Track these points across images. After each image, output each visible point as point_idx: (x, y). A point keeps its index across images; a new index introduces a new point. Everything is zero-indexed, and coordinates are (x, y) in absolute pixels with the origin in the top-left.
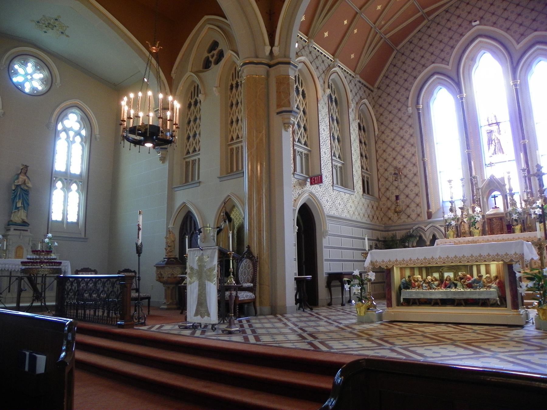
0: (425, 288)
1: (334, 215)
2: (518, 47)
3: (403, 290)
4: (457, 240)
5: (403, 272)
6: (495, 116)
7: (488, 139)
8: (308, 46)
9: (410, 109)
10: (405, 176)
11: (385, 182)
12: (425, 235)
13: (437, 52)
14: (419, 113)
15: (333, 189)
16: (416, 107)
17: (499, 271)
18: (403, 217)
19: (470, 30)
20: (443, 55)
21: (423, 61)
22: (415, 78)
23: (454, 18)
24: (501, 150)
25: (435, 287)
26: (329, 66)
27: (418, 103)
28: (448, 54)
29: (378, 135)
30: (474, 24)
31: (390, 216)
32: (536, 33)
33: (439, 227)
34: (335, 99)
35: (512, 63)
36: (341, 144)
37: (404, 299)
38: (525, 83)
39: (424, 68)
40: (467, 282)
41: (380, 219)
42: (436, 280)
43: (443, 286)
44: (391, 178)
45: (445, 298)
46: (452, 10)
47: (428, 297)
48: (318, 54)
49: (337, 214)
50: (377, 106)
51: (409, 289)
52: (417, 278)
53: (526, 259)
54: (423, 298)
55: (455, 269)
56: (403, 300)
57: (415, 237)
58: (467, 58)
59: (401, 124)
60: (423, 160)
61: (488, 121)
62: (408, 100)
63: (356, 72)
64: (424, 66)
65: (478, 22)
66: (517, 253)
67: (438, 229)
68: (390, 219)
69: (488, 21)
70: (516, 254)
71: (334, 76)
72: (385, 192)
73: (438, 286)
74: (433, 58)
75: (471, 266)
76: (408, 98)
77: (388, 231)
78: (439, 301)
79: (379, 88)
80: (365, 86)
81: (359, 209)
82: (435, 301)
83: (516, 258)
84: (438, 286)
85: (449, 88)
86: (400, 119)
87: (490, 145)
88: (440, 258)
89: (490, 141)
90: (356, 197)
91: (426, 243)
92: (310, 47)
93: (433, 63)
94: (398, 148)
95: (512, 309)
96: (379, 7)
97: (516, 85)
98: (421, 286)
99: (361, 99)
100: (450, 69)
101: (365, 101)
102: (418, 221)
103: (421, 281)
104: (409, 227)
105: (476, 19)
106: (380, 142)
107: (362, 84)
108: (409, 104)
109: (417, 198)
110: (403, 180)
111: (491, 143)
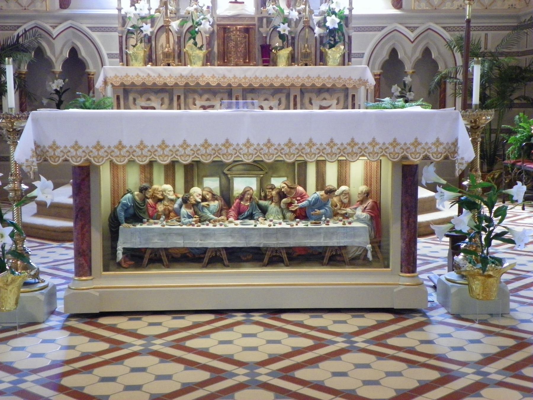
0: (187, 220)
3: (125, 225)
5: (121, 175)
17: (371, 178)
25: (212, 216)
33: (89, 31)
37: (126, 251)
40: (296, 206)
42: (214, 197)
43: (232, 213)
47: (198, 243)
51: (140, 220)
52: (164, 191)
53: (462, 158)
54: (182, 245)
55: (262, 170)
56: (123, 253)
57: (25, 50)
66: (442, 140)
70: (438, 143)
73: (219, 213)
75: (303, 165)
78: (224, 256)
82: (214, 254)
83: (437, 153)
84: (219, 213)
88: (248, 144)
91: (54, 68)
95: (401, 272)
98: (172, 214)
102: (36, 11)
103: (173, 201)
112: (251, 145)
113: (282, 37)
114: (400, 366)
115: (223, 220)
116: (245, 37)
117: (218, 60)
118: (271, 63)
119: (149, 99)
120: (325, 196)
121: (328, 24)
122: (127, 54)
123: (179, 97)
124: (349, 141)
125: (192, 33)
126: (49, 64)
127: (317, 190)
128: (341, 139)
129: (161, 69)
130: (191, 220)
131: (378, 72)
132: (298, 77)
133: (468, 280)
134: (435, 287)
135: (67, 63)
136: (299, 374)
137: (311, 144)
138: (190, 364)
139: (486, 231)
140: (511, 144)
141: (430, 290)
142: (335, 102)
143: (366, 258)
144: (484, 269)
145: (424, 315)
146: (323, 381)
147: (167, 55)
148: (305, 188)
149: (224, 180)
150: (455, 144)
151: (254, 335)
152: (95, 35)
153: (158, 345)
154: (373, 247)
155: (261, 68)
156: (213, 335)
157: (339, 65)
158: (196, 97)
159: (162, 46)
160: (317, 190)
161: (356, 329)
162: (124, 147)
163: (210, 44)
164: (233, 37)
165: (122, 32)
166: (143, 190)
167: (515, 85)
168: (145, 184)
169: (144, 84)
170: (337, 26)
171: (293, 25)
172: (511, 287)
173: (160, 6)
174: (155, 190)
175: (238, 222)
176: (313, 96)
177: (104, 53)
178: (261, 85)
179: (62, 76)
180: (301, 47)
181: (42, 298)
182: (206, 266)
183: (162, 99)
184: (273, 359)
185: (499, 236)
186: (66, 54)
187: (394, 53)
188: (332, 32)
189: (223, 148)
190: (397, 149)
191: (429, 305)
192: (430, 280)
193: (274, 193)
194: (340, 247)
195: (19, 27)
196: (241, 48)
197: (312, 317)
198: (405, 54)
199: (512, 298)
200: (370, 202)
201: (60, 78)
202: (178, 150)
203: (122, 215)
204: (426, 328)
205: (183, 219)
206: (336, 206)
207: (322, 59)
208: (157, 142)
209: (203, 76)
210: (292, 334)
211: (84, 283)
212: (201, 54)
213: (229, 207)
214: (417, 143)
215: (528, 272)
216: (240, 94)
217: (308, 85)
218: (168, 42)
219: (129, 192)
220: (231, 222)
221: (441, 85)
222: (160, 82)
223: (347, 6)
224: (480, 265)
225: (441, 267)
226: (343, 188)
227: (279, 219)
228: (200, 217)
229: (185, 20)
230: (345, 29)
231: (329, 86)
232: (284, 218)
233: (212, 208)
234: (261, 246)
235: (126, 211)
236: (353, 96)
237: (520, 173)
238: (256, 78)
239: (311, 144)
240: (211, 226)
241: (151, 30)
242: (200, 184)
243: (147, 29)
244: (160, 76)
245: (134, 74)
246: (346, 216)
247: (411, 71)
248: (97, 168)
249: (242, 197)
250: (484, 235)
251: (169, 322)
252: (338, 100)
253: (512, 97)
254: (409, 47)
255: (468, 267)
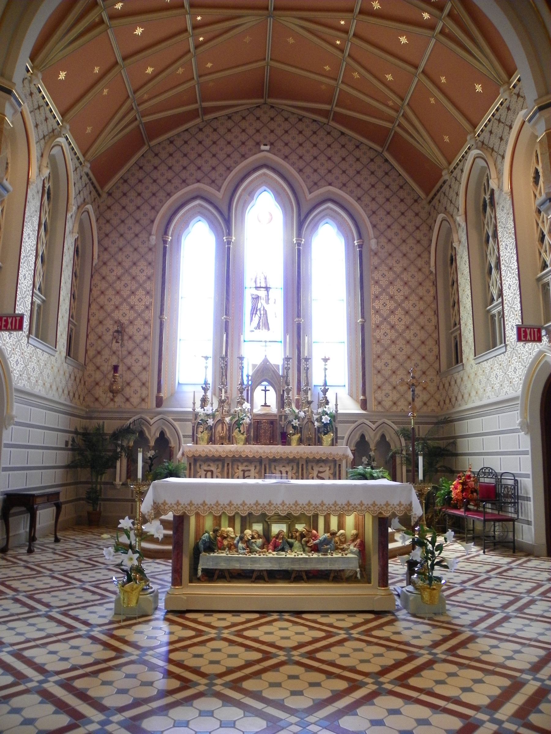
0: (242, 551)
1: (23, 389)
2: (309, 196)
3: (203, 553)
4: (214, 448)
5: (201, 521)
6: (266, 279)
7: (252, 307)
8: (30, 82)
9: (153, 238)
10: (130, 338)
11: (97, 340)
12: (149, 430)
13: (206, 168)
14: (165, 248)
15: (28, 342)
16: (163, 238)
17: (359, 525)
18: (119, 399)
19: (255, 154)
20: (213, 175)
21: (184, 175)
22: (169, 195)
23: (236, 131)
24: (267, 326)
25: (258, 549)
26: (53, 131)
27: (166, 233)
28: (221, 175)
29: (96, 265)
30: (263, 147)
31: (97, 396)
32: (330, 188)
34: (49, 190)
35: (299, 215)
36: (45, 266)
37: (203, 570)
38: (308, 244)
39: (183, 185)
40: (312, 543)
41: (82, 398)
42: (259, 537)
44: (108, 337)
45: (277, 569)
46: (237, 118)
47: (249, 566)
48: (42, 102)
49: (28, 388)
50: (102, 221)
51: (213, 551)
52: (228, 532)
53: (415, 514)
54: (238, 568)
57: (133, 432)
58: (244, 190)
59: (135, 257)
60: (160, 318)
61: (255, 282)
62: (153, 225)
63: (87, 156)
64: (184, 181)
65: (267, 148)
66: (403, 503)
67: (167, 423)
68: (97, 399)
69: (279, 150)
70: (400, 504)
71: (56, 151)
72: (95, 357)
73: (262, 547)
74: (199, 174)
75: (316, 517)
76: (152, 221)
77: (91, 418)
78: (265, 574)
79: (109, 194)
80: (92, 183)
81: (58, 379)
83: (400, 510)
84: (262, 547)
85: (212, 223)
86: (136, 249)
87: (254, 315)
88: (283, 504)
89: (254, 310)
90: (56, 360)
92: (32, 86)
93: (198, 181)
94: (125, 293)
95: (379, 586)
96: (150, 70)
97: (299, 244)
98: (232, 547)
99: (85, 202)
100: (221, 197)
101: (89, 207)
102: (142, 409)
103: (233, 539)
104: (125, 415)
105: (267, 143)
106: (97, 277)
107: (90, 179)
108: (154, 231)
109: (144, 373)
110: (125, 342)
111: (255, 312)
112: (286, 504)
113: (294, 427)
114: (382, 650)
115: (265, 552)
116: (271, 427)
117: (253, 441)
118: (287, 443)
119: (209, 465)
120: (330, 536)
121: (323, 421)
122: (197, 437)
123: (228, 464)
124: (346, 502)
125: (238, 424)
126: (147, 440)
127: (325, 532)
128: (342, 501)
129: (217, 446)
130: (244, 551)
131: (353, 448)
132: (304, 453)
133: (420, 591)
134: (398, 595)
135: (157, 441)
136: (319, 655)
137: (322, 504)
138: (248, 648)
139: (431, 560)
140: (438, 497)
141: (396, 597)
142: (328, 468)
143: (356, 577)
144: (430, 584)
145: (394, 615)
146: (334, 661)
147: (222, 438)
148: (317, 531)
149: (266, 525)
150: (411, 505)
151: (286, 629)
152: (176, 424)
153: (226, 634)
154: (361, 571)
155: (280, 446)
156: (260, 628)
157: (330, 445)
158: (239, 464)
159: (219, 432)
160: (325, 532)
161: (352, 625)
162: (206, 505)
163: (248, 431)
164: (263, 427)
165: (195, 423)
166: (215, 531)
167: (438, 459)
168: (217, 528)
169: (207, 456)
170: (328, 422)
171: (301, 420)
172: (446, 593)
173: (219, 408)
174: (223, 531)
175: (275, 553)
176: (314, 464)
177: (181, 434)
178: (281, 457)
179: (154, 448)
180: (306, 433)
181: (151, 599)
182: (253, 582)
183: (218, 465)
184: (301, 645)
185: (438, 563)
186: (158, 435)
187: (363, 437)
188: (326, 425)
189: (267, 506)
190: (376, 508)
191: (396, 607)
192: (395, 590)
193: (297, 534)
194: (340, 571)
195: (130, 418)
196: (268, 434)
197: (322, 616)
198: (370, 438)
199: (447, 602)
200: (358, 541)
201: (153, 449)
202: (239, 507)
203: (202, 547)
204: (396, 623)
205: (240, 551)
206: (337, 543)
207: (319, 442)
208: (226, 502)
209: (244, 451)
210: (311, 628)
211: (177, 590)
212: (243, 437)
213: (269, 543)
214: (387, 504)
215: (455, 583)
216: (267, 462)
217: (311, 458)
218: (223, 429)
219: (206, 532)
220: (270, 553)
221: (393, 457)
222: (217, 455)
223: (335, 410)
224: (427, 582)
225: (401, 581)
226: (342, 531)
227: (301, 551)
228: (251, 549)
229: (234, 416)
230: (333, 423)
231: (324, 458)
232: (304, 551)
233: (258, 543)
234: (289, 569)
235: (204, 544)
236: (340, 465)
237: (444, 515)
238: (278, 453)
239: (322, 504)
240: (257, 556)
241: (213, 422)
242: (250, 528)
243: (211, 422)
244: (217, 451)
245: (201, 450)
246: (343, 550)
247: (374, 448)
248: (188, 517)
249: (277, 536)
250: (430, 562)
251: (231, 619)
252: (330, 467)
253: (437, 466)
254: (372, 434)
255: (420, 583)
